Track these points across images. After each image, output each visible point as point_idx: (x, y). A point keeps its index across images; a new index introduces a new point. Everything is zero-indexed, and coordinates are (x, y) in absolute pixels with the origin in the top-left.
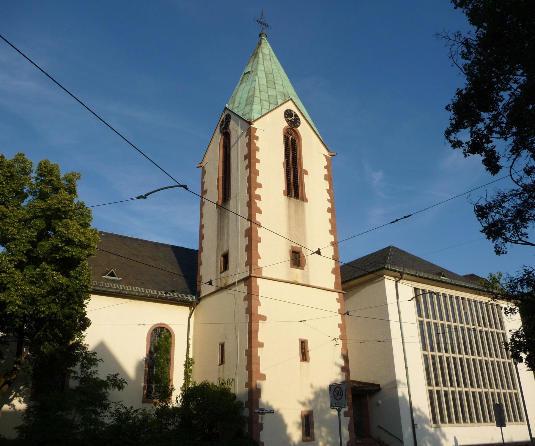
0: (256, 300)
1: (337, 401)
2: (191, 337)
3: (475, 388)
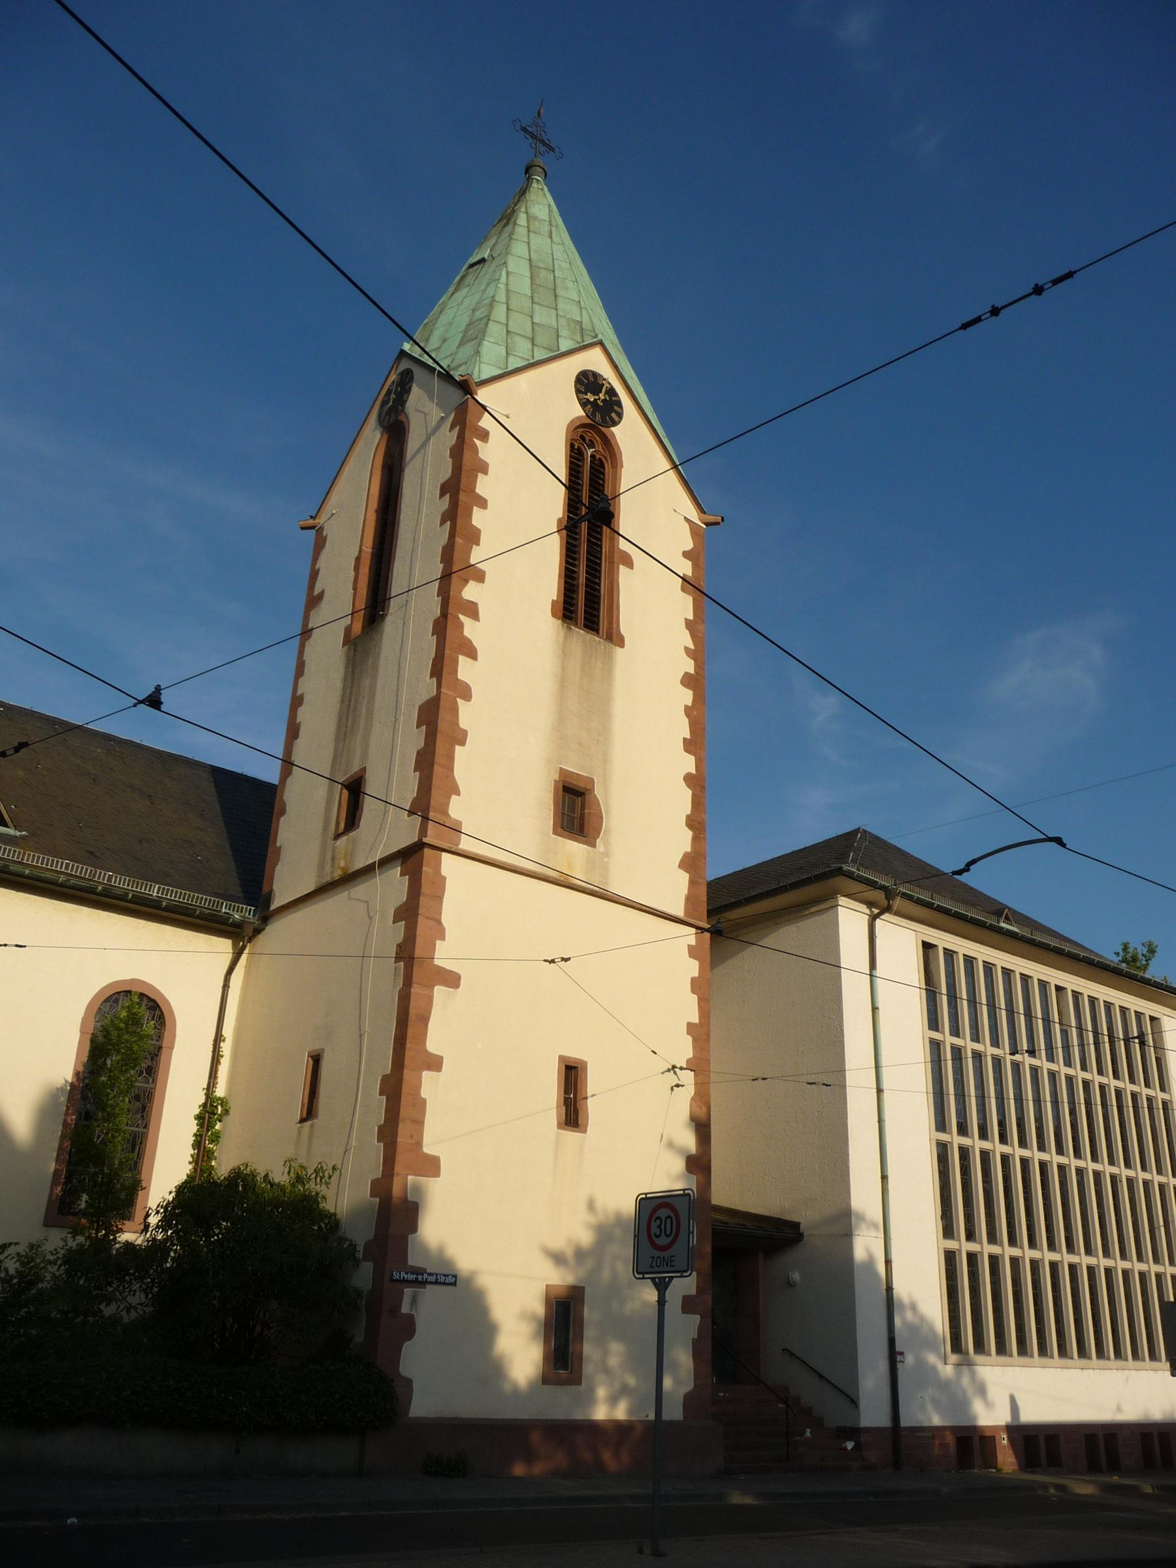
0: (432, 919)
1: (656, 1253)
2: (228, 1031)
3: (1079, 1254)
